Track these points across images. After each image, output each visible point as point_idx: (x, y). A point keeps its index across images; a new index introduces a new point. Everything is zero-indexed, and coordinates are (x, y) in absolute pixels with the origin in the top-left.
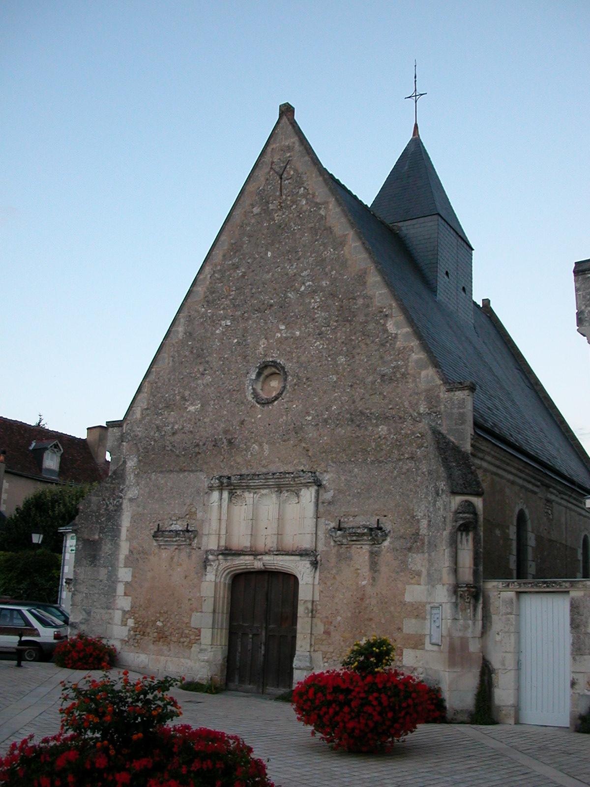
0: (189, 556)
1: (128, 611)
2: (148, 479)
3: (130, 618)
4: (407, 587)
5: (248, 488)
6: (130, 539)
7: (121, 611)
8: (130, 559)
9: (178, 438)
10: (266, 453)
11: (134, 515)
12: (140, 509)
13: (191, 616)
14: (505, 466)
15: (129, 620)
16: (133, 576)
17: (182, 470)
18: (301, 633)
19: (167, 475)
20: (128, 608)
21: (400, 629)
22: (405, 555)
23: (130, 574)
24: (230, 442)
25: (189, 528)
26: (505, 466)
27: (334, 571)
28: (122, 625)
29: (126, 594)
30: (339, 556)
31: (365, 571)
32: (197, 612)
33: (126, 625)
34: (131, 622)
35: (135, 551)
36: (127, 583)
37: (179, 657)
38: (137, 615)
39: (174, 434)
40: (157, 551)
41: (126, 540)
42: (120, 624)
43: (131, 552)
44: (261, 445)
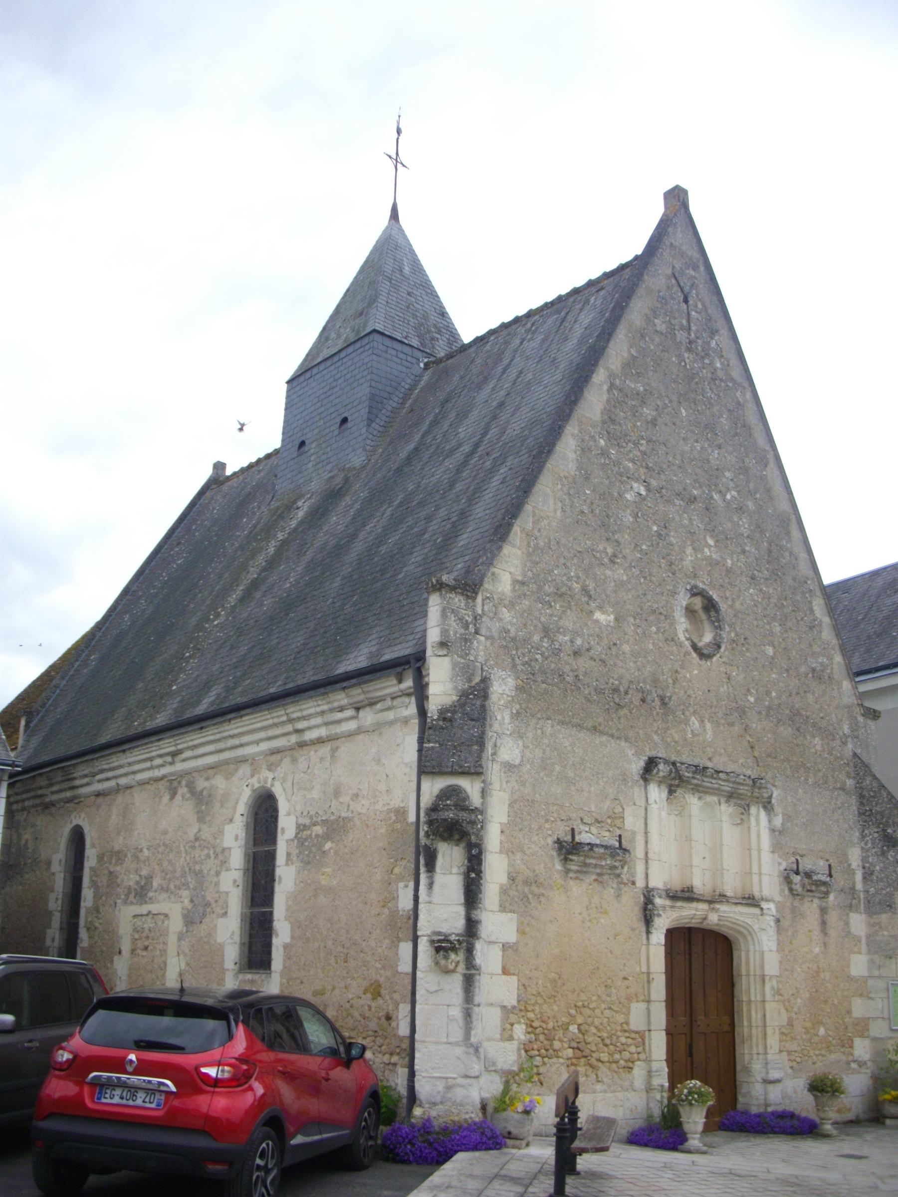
0: (618, 896)
1: (514, 1007)
2: (539, 732)
3: (519, 1022)
4: (852, 956)
5: (697, 789)
6: (508, 850)
7: (499, 1010)
8: (511, 893)
9: (583, 663)
10: (709, 736)
11: (515, 801)
12: (527, 790)
13: (629, 1009)
14: (221, 745)
15: (516, 1026)
16: (521, 932)
17: (595, 729)
18: (93, 846)
19: (573, 733)
20: (511, 1000)
21: (849, 1012)
22: (847, 915)
23: (514, 927)
24: (662, 699)
25: (577, 839)
26: (221, 745)
27: (790, 933)
28: (502, 1039)
29: (505, 971)
30: (793, 909)
31: (816, 933)
32: (637, 1001)
33: (511, 1038)
34: (520, 1031)
35: (520, 879)
36: (505, 947)
37: (615, 1092)
38: (531, 1015)
39: (576, 654)
40: (560, 881)
41: (501, 852)
42: (498, 1036)
43: (512, 879)
44: (702, 722)
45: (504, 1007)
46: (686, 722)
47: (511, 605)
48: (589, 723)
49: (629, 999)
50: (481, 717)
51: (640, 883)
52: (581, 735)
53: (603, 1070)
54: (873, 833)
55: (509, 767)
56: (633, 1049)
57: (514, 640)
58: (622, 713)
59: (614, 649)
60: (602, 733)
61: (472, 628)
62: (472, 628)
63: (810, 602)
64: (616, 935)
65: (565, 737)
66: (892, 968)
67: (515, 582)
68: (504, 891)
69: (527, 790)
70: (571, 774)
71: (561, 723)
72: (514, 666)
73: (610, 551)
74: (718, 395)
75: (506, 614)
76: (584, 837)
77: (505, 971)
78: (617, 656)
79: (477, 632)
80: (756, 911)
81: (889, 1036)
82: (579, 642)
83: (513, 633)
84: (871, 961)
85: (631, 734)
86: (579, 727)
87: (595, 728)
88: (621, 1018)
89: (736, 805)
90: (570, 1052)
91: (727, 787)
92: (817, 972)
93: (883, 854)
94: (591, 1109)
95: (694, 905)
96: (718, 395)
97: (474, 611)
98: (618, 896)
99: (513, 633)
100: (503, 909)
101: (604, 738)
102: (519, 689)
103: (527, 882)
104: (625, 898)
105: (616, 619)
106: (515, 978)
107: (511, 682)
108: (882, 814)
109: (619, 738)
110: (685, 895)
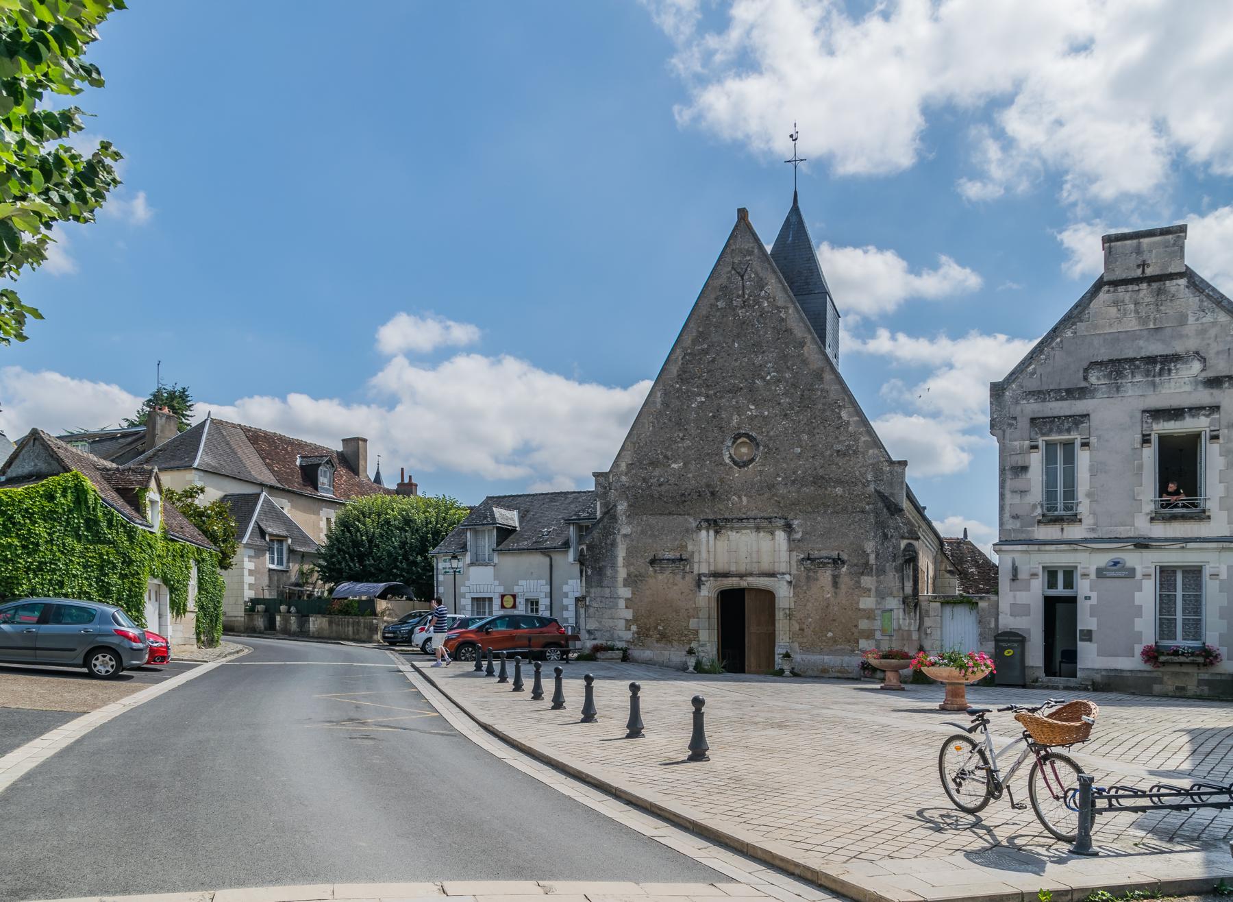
0: (683, 578)
6: (627, 564)
16: (633, 593)
21: (856, 626)
23: (630, 592)
29: (627, 607)
33: (630, 630)
34: (634, 628)
36: (627, 599)
44: (740, 497)
45: (626, 620)
46: (729, 499)
47: (626, 474)
48: (667, 512)
49: (689, 617)
50: (614, 518)
51: (696, 572)
52: (662, 517)
53: (675, 643)
54: (880, 533)
55: (625, 536)
56: (691, 636)
57: (628, 488)
58: (686, 504)
59: (682, 478)
60: (674, 514)
61: (608, 488)
62: (608, 488)
63: (839, 413)
64: (682, 593)
65: (652, 520)
66: (6, 571)
67: (628, 465)
68: (625, 580)
69: (634, 543)
70: (657, 533)
71: (650, 515)
72: (627, 497)
73: (681, 435)
74: (765, 324)
75: (624, 478)
76: (660, 556)
77: (627, 607)
78: (684, 480)
79: (610, 489)
80: (776, 579)
81: (1142, 669)
82: (662, 480)
83: (627, 485)
84: (877, 601)
85: (691, 511)
86: (661, 514)
87: (670, 513)
88: (685, 624)
89: (764, 532)
90: (658, 636)
91: (752, 525)
92: (827, 607)
93: (883, 544)
94: (544, 602)
95: (730, 579)
96: (765, 324)
97: (608, 481)
98: (683, 578)
99: (627, 485)
100: (625, 586)
101: (675, 516)
102: (630, 506)
103: (636, 576)
104: (687, 578)
105: (684, 464)
106: (631, 610)
107: (626, 504)
108: (883, 522)
109: (684, 515)
110: (716, 575)
